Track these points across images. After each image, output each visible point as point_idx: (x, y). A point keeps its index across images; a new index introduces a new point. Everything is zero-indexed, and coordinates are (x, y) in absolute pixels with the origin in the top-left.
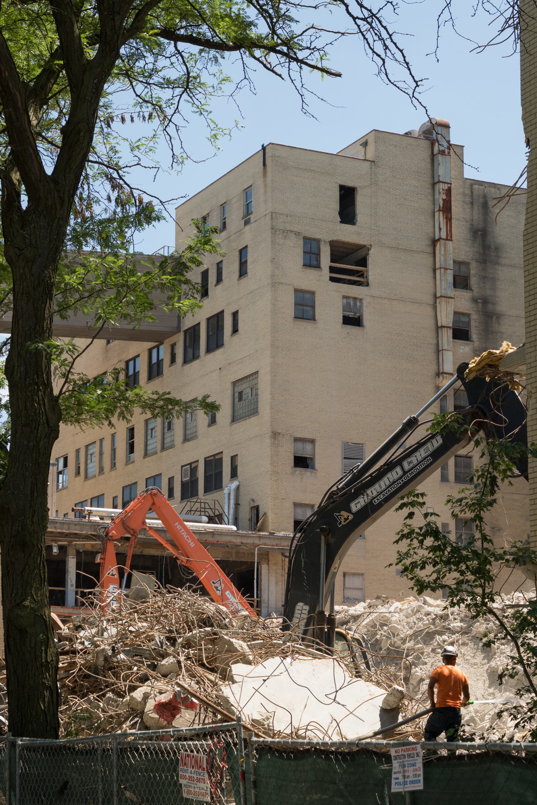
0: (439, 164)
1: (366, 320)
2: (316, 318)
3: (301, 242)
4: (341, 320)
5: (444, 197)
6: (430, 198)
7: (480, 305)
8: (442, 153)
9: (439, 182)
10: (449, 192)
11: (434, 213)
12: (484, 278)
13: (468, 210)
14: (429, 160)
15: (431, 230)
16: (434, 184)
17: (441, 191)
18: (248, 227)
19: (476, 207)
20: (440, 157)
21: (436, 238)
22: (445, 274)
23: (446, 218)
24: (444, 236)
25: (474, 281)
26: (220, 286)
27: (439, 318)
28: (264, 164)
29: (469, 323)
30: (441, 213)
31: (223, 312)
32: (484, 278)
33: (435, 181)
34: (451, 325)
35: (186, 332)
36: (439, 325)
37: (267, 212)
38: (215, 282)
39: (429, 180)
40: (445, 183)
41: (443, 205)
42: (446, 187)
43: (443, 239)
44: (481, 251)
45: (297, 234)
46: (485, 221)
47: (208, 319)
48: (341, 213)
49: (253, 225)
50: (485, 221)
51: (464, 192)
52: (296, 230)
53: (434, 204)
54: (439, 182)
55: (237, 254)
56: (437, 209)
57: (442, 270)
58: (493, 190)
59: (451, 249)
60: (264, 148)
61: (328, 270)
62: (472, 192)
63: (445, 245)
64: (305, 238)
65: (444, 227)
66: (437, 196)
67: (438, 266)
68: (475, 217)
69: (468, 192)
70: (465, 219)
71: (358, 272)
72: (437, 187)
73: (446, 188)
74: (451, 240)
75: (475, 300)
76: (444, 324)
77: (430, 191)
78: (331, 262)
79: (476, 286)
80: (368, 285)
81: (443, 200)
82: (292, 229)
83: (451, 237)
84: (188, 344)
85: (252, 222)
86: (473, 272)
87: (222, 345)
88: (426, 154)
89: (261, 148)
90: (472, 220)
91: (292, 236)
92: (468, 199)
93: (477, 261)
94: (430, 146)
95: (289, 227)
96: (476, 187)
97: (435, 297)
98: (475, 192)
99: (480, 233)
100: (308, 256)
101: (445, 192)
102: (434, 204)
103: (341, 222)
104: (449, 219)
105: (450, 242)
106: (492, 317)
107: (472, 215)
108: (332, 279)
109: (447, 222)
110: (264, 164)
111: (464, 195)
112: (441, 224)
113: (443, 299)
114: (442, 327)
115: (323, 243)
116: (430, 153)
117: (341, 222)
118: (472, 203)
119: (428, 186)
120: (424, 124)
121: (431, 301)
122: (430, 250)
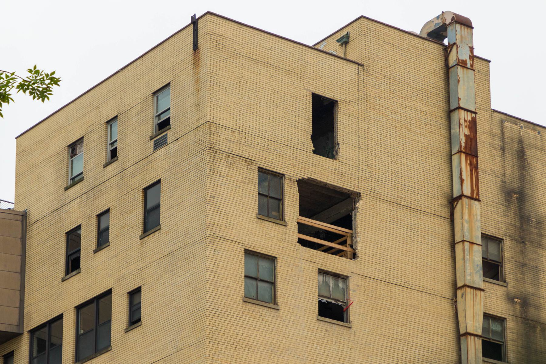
0: (459, 81)
1: (354, 312)
2: (279, 300)
3: (255, 175)
4: (316, 308)
5: (467, 132)
6: (444, 132)
7: (518, 307)
8: (462, 64)
9: (459, 108)
10: (473, 126)
11: (451, 156)
12: (522, 266)
13: (498, 159)
14: (441, 74)
15: (447, 182)
16: (449, 112)
17: (462, 121)
18: (161, 152)
19: (508, 156)
20: (460, 69)
21: (455, 195)
22: (470, 249)
23: (471, 164)
24: (467, 191)
25: (509, 268)
26: (104, 253)
27: (461, 319)
28: (196, 47)
29: (502, 333)
30: (463, 156)
31: (109, 292)
32: (523, 265)
33: (452, 108)
34: (480, 332)
35: (32, 332)
36: (462, 331)
37: (202, 122)
38: (94, 246)
39: (442, 104)
40: (468, 111)
41: (466, 143)
42: (469, 117)
43: (467, 197)
44: (518, 224)
45: (249, 161)
46: (522, 178)
47: (79, 308)
48: (314, 138)
49: (171, 146)
50: (522, 178)
51: (491, 130)
52: (246, 155)
53: (450, 143)
54: (459, 108)
55: (140, 196)
56: (455, 150)
57: (466, 244)
58: (532, 133)
59: (478, 213)
60: (195, 22)
61: (295, 228)
62: (503, 133)
63: (470, 206)
64: (261, 170)
65: (466, 176)
66: (455, 130)
67: (458, 238)
68: (508, 172)
69: (497, 131)
70: (494, 172)
71: (340, 236)
72: (455, 116)
73: (470, 118)
74: (479, 200)
75: (510, 299)
76: (470, 330)
77: (443, 121)
78: (301, 214)
79: (511, 276)
80: (354, 256)
81: (466, 136)
82: (241, 153)
83: (478, 194)
84: (35, 354)
85: (168, 141)
86: (507, 254)
87: (107, 348)
88: (438, 65)
89: (189, 21)
90: (504, 176)
91: (241, 164)
92: (498, 143)
93: (513, 239)
94: (442, 53)
95: (235, 149)
96: (507, 124)
97: (455, 288)
98: (507, 134)
99: (515, 196)
100: (265, 200)
101: (468, 124)
102: (450, 143)
103: (314, 152)
104: (474, 167)
105: (477, 203)
106: (535, 327)
107: (504, 167)
108: (301, 242)
109: (471, 171)
110: (196, 47)
111: (493, 135)
112: (464, 173)
113: (468, 290)
114: (467, 334)
115: (287, 181)
116: (442, 63)
117: (314, 152)
118: (503, 149)
119: (440, 112)
120: (431, 21)
121: (447, 292)
122: (445, 212)
